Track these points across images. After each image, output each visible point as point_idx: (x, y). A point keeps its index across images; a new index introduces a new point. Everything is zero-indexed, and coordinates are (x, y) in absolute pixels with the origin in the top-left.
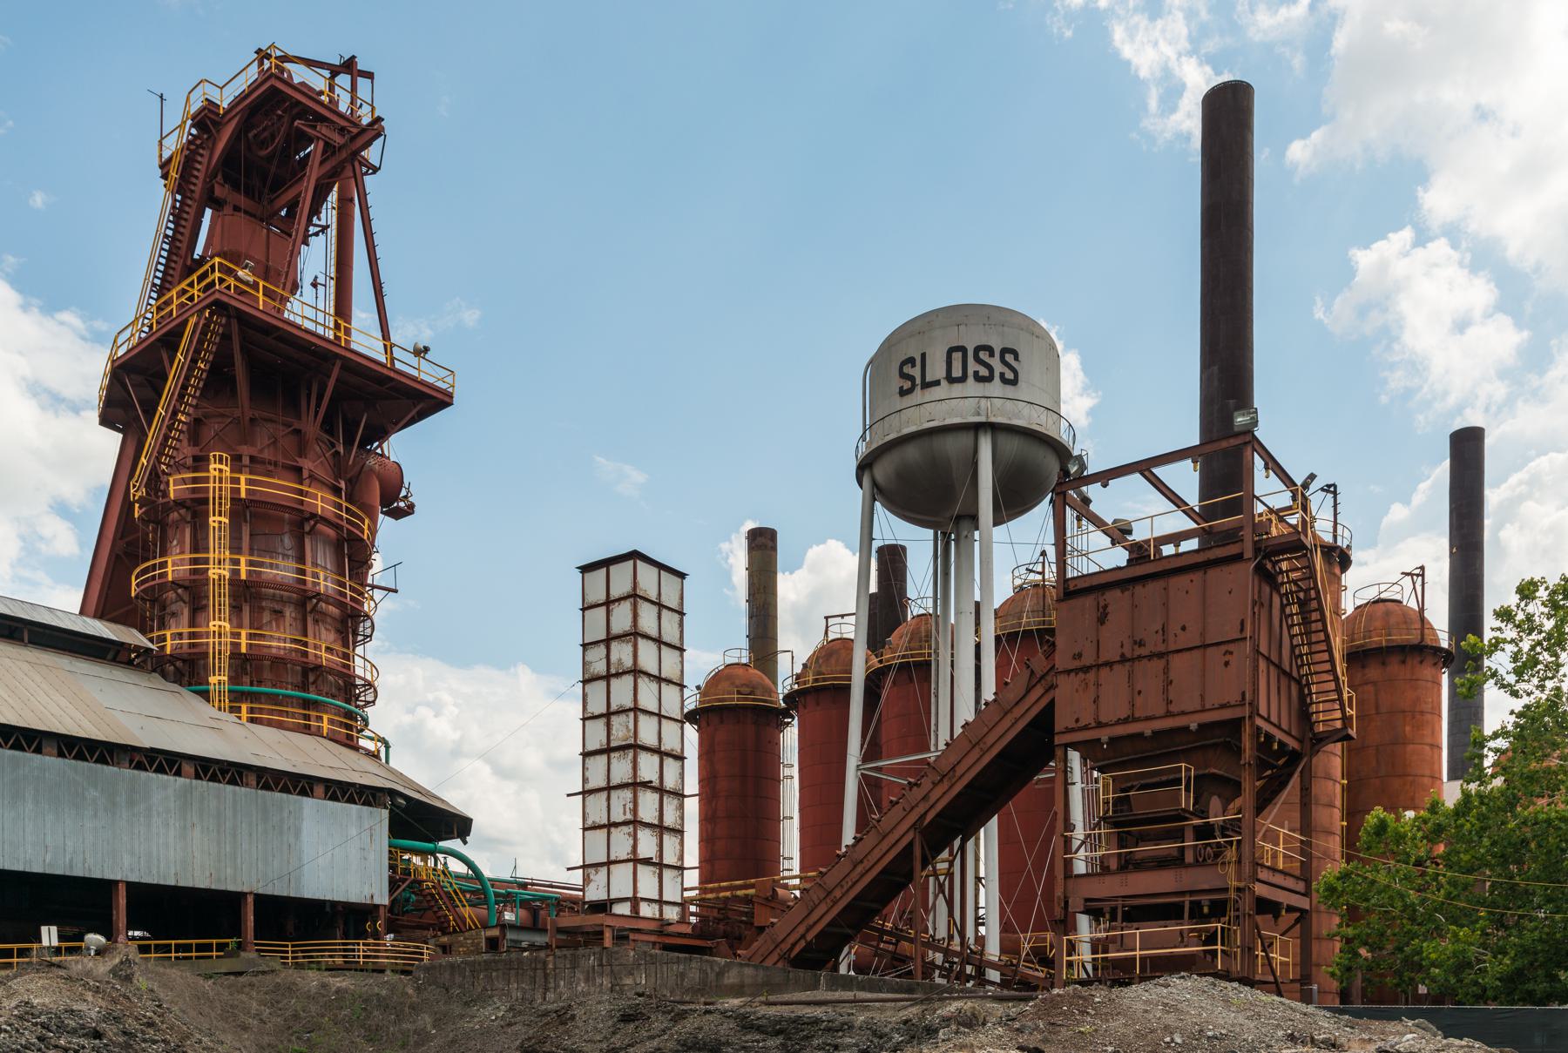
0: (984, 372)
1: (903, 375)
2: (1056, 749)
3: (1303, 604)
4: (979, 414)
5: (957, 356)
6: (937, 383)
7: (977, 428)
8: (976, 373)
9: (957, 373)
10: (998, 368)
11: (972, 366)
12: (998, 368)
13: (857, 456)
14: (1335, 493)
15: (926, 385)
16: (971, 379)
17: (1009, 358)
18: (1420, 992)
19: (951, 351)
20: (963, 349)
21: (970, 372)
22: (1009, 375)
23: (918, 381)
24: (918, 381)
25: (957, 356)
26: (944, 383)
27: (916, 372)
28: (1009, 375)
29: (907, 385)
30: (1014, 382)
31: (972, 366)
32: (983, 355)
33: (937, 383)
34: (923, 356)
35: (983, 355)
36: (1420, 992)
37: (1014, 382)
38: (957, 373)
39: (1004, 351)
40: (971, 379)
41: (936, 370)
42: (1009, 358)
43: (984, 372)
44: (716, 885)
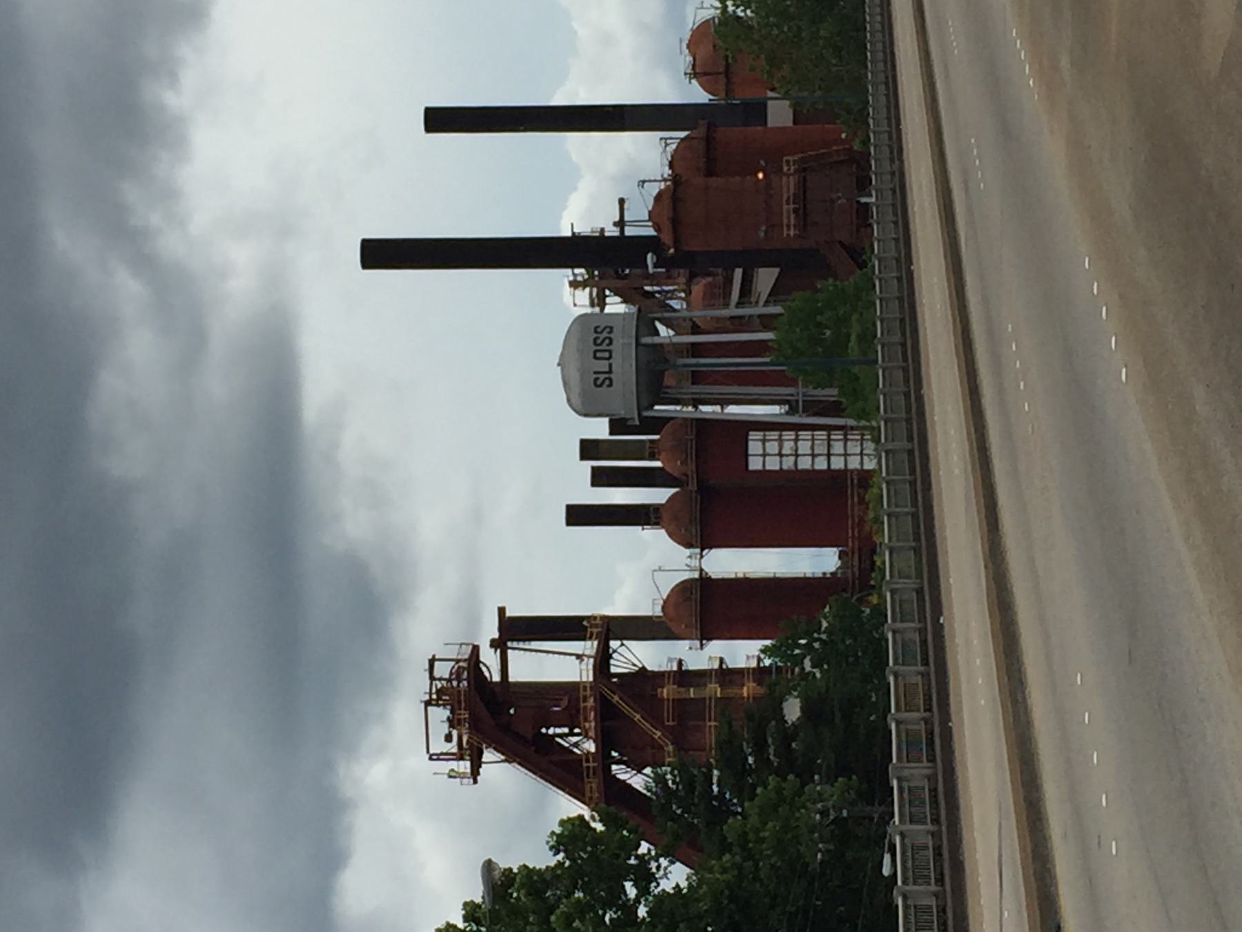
0: (607, 341)
1: (601, 386)
2: (833, 467)
3: (745, 770)
4: (630, 344)
5: (599, 355)
6: (610, 365)
7: (638, 344)
8: (608, 345)
9: (607, 355)
10: (605, 334)
11: (604, 347)
12: (605, 334)
13: (485, 665)
14: (644, 182)
15: (610, 372)
16: (595, 335)
17: (599, 330)
18: (755, 464)
19: (595, 358)
20: (595, 352)
21: (608, 348)
22: (608, 330)
23: (607, 376)
24: (607, 376)
25: (599, 355)
26: (611, 361)
27: (602, 377)
28: (608, 330)
29: (607, 382)
30: (611, 328)
31: (604, 347)
32: (599, 342)
33: (610, 365)
34: (596, 373)
35: (599, 342)
36: (755, 464)
37: (611, 328)
38: (607, 355)
39: (596, 332)
40: (595, 335)
41: (603, 366)
42: (599, 330)
43: (607, 341)
44: (850, 540)
